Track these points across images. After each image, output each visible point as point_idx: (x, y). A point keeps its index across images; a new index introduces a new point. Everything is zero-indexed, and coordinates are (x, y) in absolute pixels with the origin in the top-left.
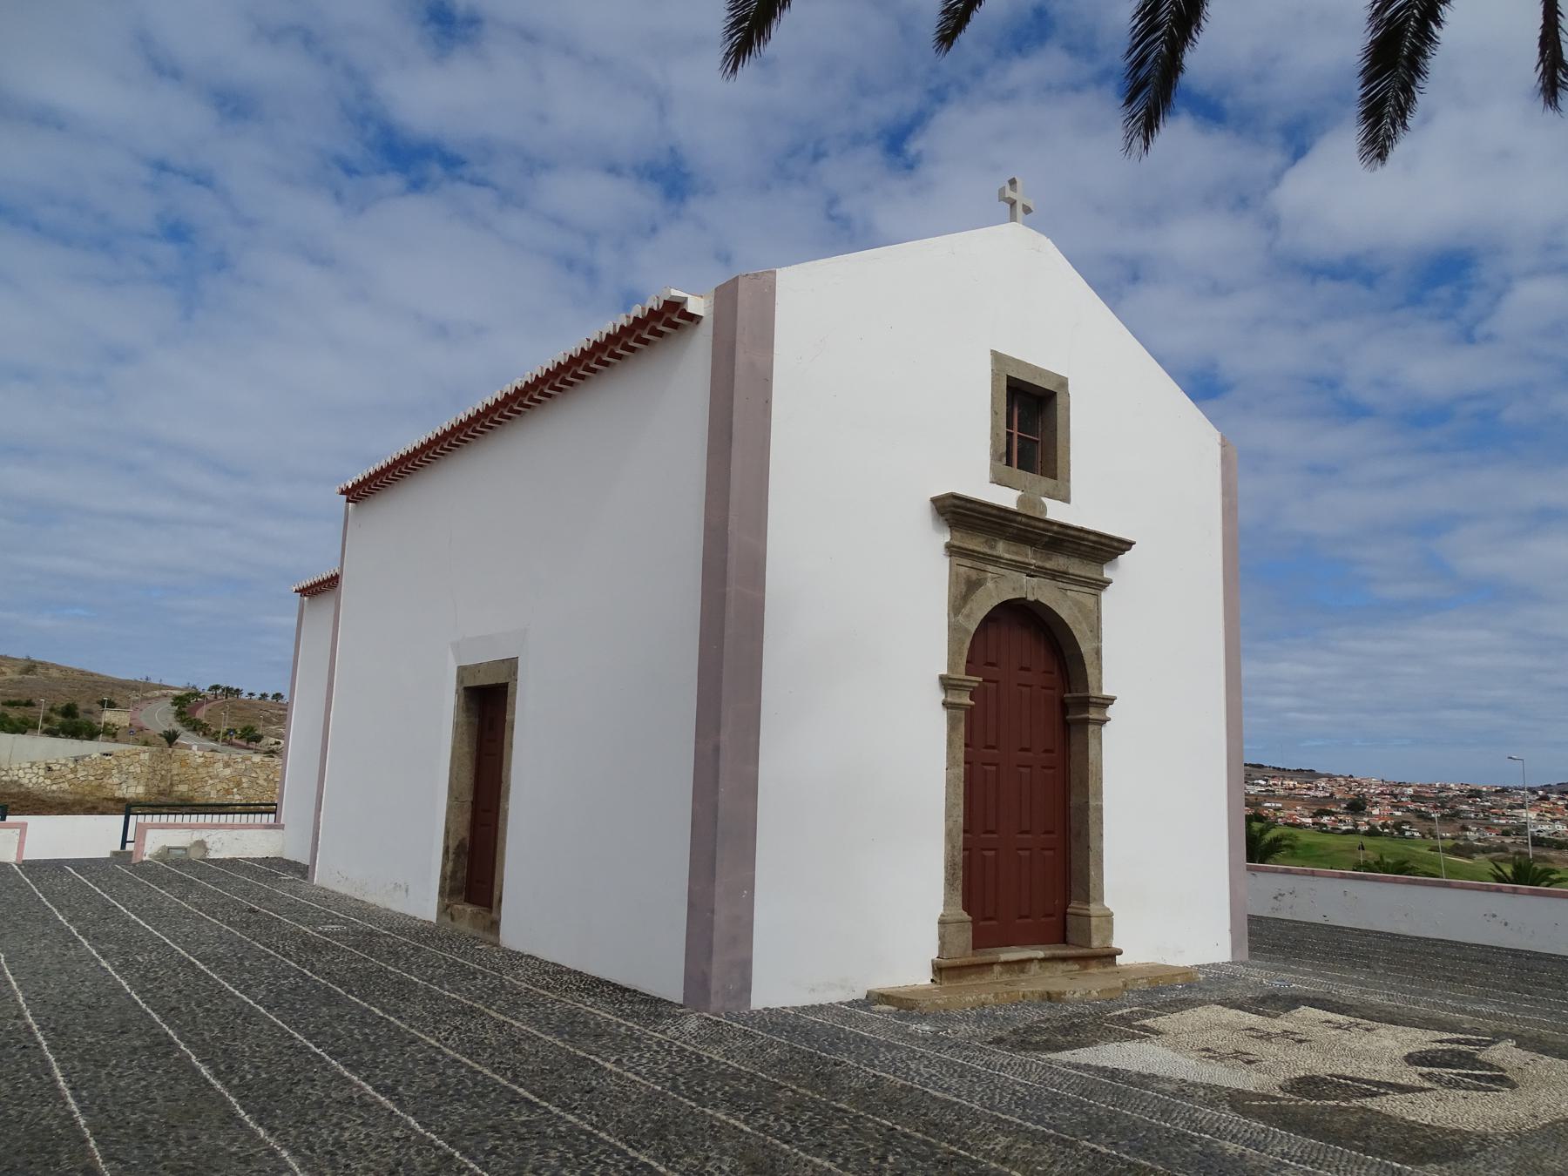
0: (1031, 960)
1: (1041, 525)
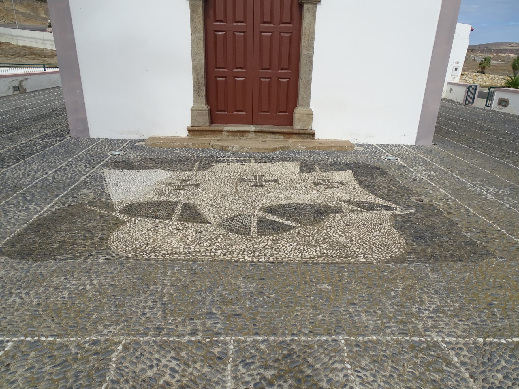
0: (249, 132)
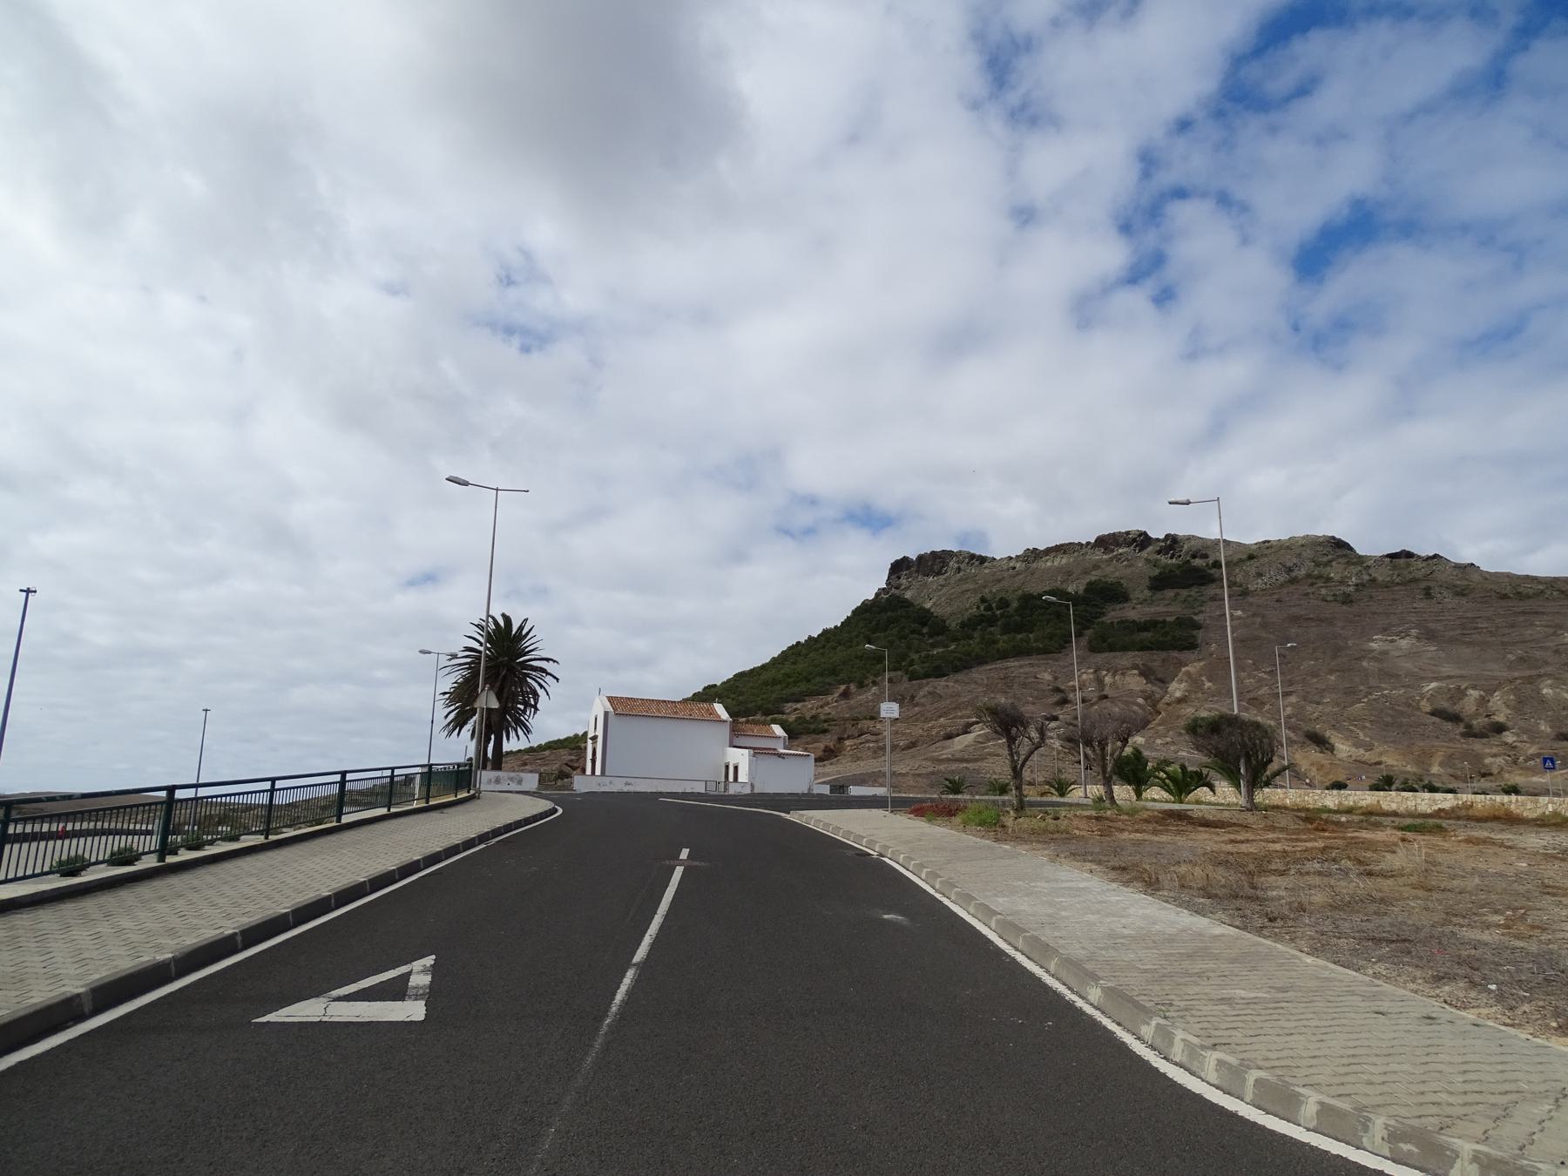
1: (1061, 561)
